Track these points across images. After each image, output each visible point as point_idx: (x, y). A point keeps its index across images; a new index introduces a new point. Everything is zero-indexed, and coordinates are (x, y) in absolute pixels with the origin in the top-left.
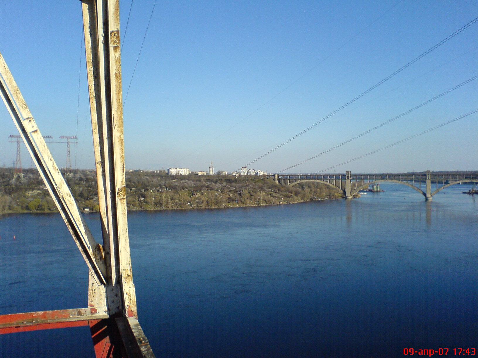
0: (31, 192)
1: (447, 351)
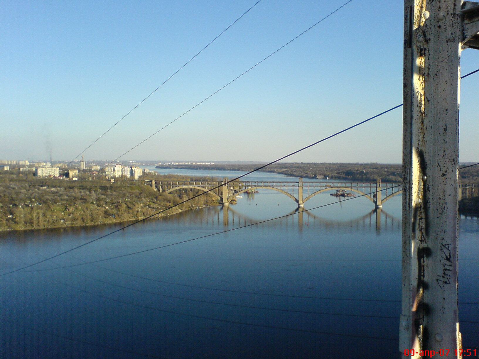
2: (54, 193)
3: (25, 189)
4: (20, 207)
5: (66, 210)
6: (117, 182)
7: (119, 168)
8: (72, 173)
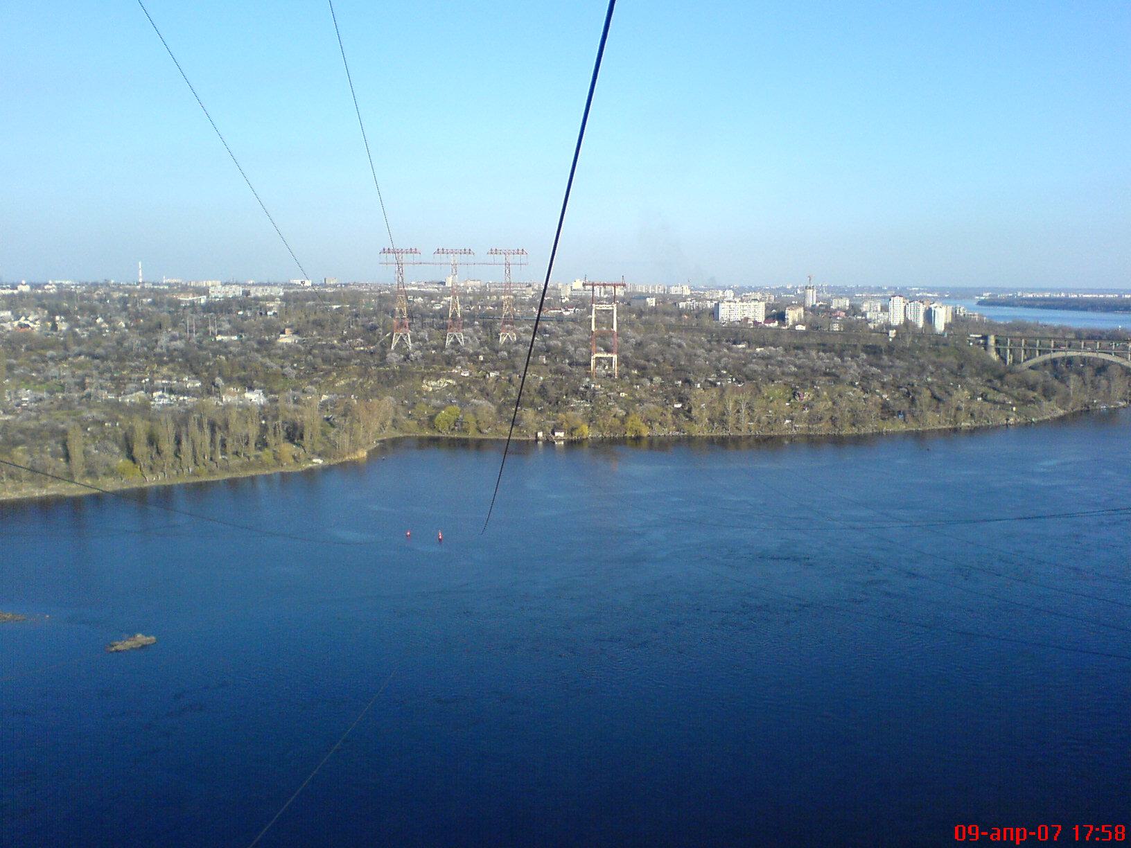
0: (433, 383)
1: (1058, 832)
2: (763, 358)
3: (702, 346)
4: (699, 386)
5: (794, 397)
6: (903, 337)
7: (898, 304)
8: (792, 315)
